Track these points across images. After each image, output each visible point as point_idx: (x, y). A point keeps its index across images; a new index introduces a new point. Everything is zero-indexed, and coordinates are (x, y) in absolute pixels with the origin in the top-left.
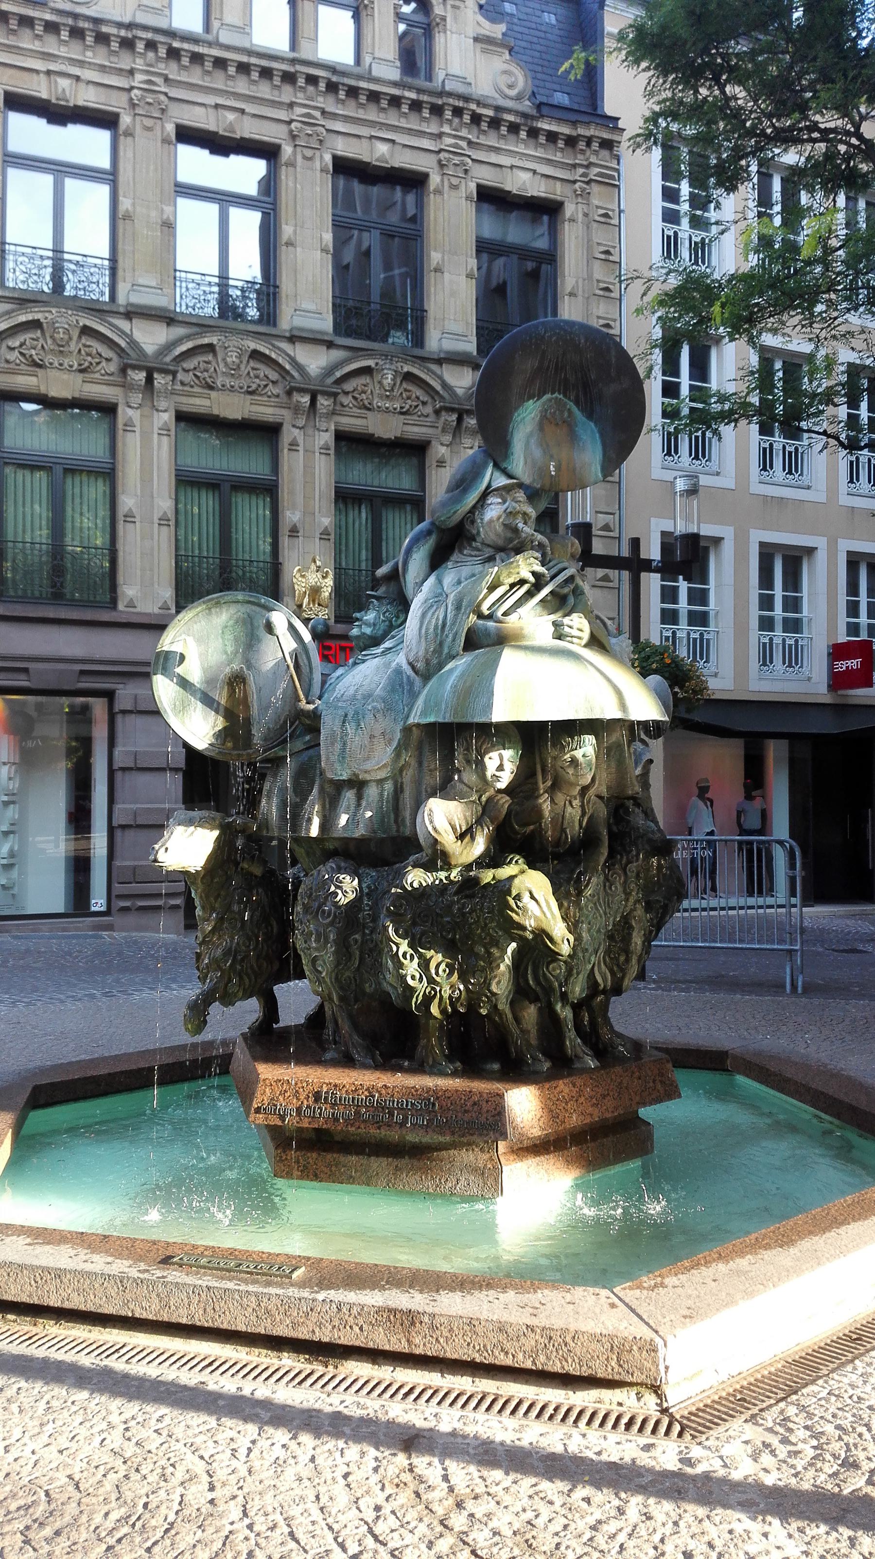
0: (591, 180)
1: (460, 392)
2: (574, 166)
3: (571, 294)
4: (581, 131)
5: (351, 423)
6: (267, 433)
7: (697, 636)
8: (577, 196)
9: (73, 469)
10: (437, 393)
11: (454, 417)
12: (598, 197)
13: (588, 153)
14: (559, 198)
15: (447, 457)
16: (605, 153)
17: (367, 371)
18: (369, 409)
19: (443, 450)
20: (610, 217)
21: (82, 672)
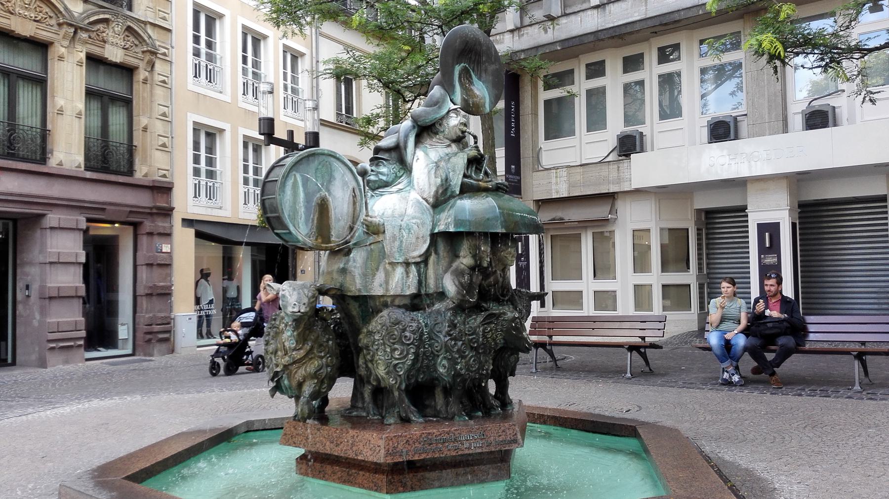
1: (76, 15)
5: (96, 50)
6: (41, 47)
7: (211, 184)
9: (114, 99)
10: (61, 12)
11: (72, 30)
15: (65, 55)
17: (106, 21)
18: (12, 14)
19: (63, 50)
21: (131, 212)
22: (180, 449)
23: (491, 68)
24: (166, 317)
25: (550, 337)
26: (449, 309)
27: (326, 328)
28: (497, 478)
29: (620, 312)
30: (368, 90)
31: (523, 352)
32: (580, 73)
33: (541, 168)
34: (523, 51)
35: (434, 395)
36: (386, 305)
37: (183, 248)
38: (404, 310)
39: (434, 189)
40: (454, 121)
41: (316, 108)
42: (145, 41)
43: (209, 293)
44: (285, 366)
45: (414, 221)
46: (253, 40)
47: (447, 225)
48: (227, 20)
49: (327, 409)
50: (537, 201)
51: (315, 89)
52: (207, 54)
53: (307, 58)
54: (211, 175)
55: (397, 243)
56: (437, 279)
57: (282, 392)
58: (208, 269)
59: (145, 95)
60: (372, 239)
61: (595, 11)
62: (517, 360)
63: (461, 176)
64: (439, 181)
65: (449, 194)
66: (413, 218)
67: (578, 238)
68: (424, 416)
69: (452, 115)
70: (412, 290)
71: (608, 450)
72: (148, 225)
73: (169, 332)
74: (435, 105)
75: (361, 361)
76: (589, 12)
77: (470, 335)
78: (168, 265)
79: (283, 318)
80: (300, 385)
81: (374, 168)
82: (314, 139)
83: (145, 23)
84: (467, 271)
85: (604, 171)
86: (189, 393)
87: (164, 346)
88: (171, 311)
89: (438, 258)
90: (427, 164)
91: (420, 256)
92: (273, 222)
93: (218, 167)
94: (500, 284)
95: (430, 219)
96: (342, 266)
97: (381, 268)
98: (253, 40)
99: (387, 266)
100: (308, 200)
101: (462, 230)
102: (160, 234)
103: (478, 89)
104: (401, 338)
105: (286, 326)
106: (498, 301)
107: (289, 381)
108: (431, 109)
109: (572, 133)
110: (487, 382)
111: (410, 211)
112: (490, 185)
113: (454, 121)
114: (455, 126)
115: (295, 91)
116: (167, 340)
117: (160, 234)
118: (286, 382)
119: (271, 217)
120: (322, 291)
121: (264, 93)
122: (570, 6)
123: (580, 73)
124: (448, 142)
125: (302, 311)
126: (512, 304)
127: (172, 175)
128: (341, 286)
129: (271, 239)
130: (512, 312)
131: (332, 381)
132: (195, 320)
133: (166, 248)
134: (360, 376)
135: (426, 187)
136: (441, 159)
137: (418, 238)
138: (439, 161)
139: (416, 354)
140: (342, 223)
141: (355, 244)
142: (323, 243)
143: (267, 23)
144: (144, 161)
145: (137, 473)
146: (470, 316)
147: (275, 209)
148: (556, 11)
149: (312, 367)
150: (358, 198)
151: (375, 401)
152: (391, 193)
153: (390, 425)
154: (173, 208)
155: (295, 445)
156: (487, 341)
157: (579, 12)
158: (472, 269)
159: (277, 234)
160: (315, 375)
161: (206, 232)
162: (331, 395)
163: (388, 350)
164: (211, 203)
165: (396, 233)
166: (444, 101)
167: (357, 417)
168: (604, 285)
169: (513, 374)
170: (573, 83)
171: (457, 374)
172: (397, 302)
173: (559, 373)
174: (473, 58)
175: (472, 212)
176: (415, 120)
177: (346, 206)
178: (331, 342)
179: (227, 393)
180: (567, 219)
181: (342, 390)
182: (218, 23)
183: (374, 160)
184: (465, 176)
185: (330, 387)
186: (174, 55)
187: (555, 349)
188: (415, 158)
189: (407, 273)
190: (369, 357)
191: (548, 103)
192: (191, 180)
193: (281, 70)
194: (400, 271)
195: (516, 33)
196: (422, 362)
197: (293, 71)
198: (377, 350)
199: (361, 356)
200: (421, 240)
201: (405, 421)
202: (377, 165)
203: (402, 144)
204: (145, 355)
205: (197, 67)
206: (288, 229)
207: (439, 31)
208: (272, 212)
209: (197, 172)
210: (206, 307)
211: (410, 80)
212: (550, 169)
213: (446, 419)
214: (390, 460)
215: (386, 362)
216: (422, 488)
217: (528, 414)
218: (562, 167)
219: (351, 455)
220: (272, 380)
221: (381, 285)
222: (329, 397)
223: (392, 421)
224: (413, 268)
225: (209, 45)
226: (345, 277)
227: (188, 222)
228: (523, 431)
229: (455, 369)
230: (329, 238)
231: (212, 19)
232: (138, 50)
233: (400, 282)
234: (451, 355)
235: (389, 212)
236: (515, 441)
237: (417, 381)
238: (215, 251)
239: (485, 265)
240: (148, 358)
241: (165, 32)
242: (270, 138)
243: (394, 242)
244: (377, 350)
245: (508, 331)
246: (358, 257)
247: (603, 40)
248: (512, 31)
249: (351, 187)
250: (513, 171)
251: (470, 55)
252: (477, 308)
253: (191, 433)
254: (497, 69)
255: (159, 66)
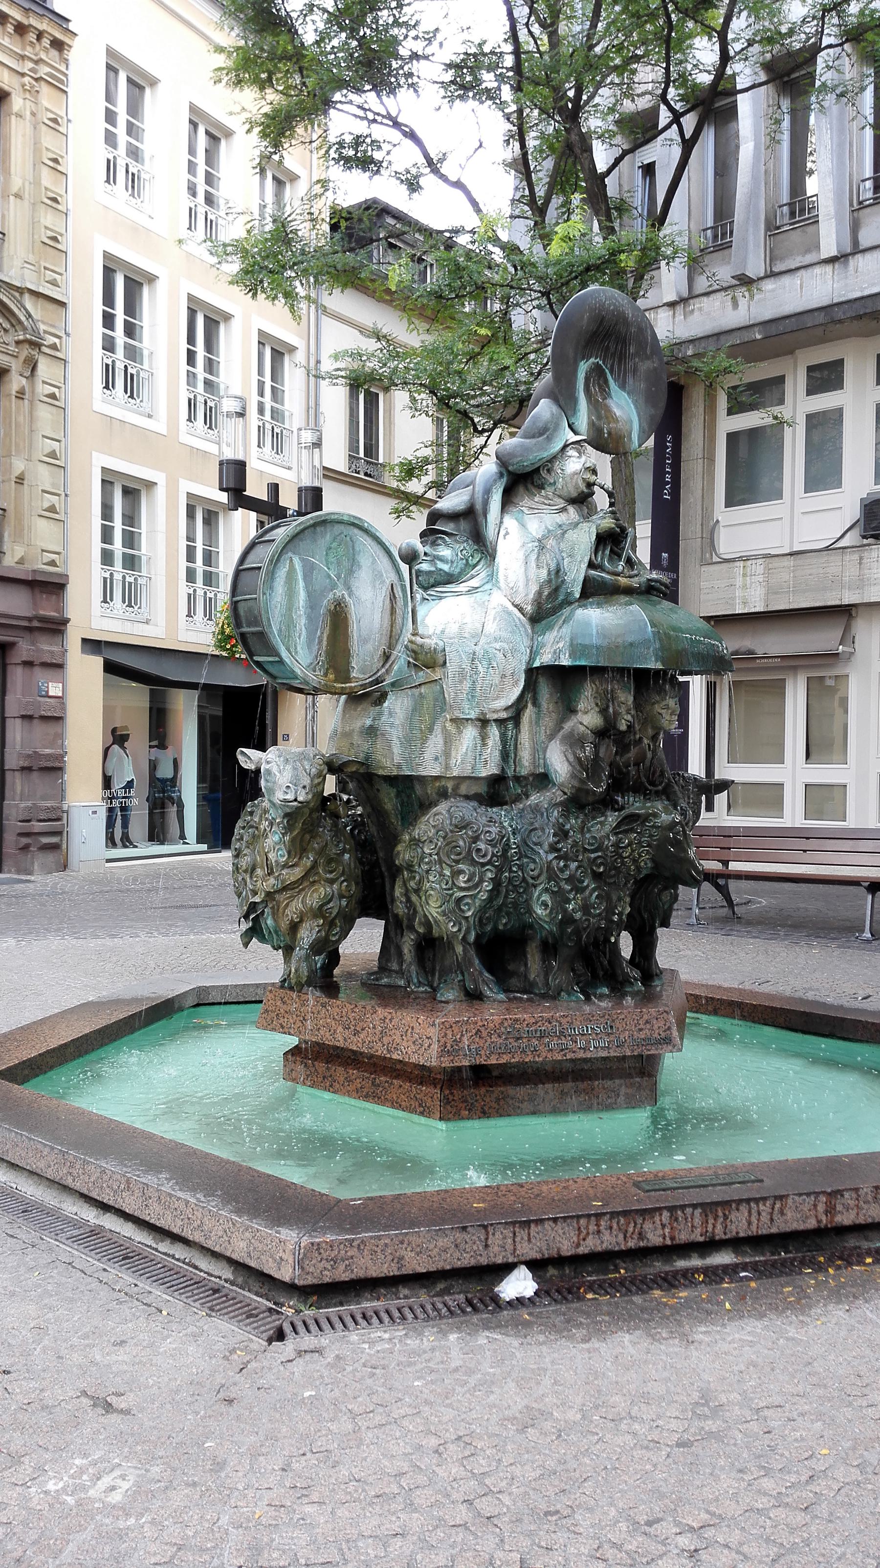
0: (41, 78)
2: (23, 57)
3: (17, 196)
4: (33, 21)
7: (132, 580)
8: (25, 90)
12: (47, 97)
13: (38, 47)
14: (6, 88)
16: (54, 53)
20: (58, 124)
22: (87, 1031)
23: (645, 366)
24: (54, 809)
25: (726, 863)
26: (556, 805)
27: (337, 831)
28: (632, 1104)
29: (852, 822)
30: (408, 413)
31: (685, 884)
32: (796, 383)
33: (715, 559)
34: (692, 341)
35: (524, 954)
36: (443, 794)
37: (83, 693)
38: (476, 804)
39: (534, 588)
40: (573, 464)
41: (318, 444)
42: (20, 322)
43: (128, 768)
44: (269, 894)
45: (498, 645)
46: (206, 324)
47: (557, 654)
48: (161, 286)
49: (336, 971)
50: (708, 619)
51: (312, 412)
52: (127, 347)
53: (300, 356)
54: (131, 562)
55: (467, 685)
56: (534, 751)
57: (262, 939)
58: (126, 728)
59: (21, 419)
60: (421, 676)
61: (829, 268)
62: (675, 898)
63: (584, 566)
64: (544, 574)
65: (561, 598)
66: (496, 640)
67: (778, 689)
68: (506, 991)
69: (571, 452)
70: (491, 769)
71: (830, 1063)
72: (24, 648)
73: (59, 833)
74: (541, 435)
75: (398, 892)
76: (818, 270)
77: (593, 851)
78: (59, 719)
79: (266, 811)
80: (294, 927)
81: (427, 549)
82: (313, 498)
83: (21, 290)
84: (591, 737)
85: (834, 565)
86: (97, 937)
87: (50, 858)
88: (63, 798)
89: (538, 714)
90: (525, 543)
91: (507, 709)
92: (251, 641)
93: (144, 549)
94: (647, 762)
95: (527, 642)
96: (368, 722)
97: (438, 729)
98: (206, 324)
99: (448, 724)
100: (312, 605)
101: (583, 663)
102: (45, 665)
103: (618, 406)
104: (469, 852)
105: (271, 824)
106: (638, 789)
107: (275, 920)
108: (534, 441)
109: (778, 494)
110: (619, 935)
111: (491, 628)
112: (635, 582)
113: (573, 464)
114: (575, 473)
115: (277, 415)
116: (56, 847)
117: (45, 665)
118: (270, 922)
119: (246, 632)
120: (332, 767)
121: (229, 415)
122: (782, 259)
123: (796, 383)
124: (562, 504)
125: (300, 799)
126: (668, 799)
127: (65, 562)
128: (367, 758)
129: (237, 678)
130: (668, 812)
131: (346, 922)
132: (103, 814)
133: (55, 689)
134: (396, 916)
135: (521, 584)
136: (549, 533)
137: (503, 676)
138: (545, 537)
139: (497, 882)
140: (369, 647)
141: (393, 684)
142: (336, 680)
143: (235, 288)
144: (19, 535)
145: (16, 1066)
146: (594, 818)
147: (256, 620)
148: (755, 267)
149: (314, 897)
150: (400, 602)
151: (420, 962)
152: (459, 594)
153: (447, 1002)
154: (67, 621)
155: (284, 1030)
156: (623, 863)
157: (798, 269)
158: (601, 734)
159: (258, 664)
160: (319, 912)
161: (122, 664)
162: (345, 948)
163: (447, 873)
164: (130, 613)
165: (466, 666)
166: (557, 427)
167: (389, 986)
168: (823, 774)
169: (665, 924)
170: (781, 402)
171: (568, 920)
172: (464, 789)
173: (738, 927)
174: (612, 350)
175: (603, 633)
176: (502, 460)
177: (377, 617)
178: (347, 856)
179: (160, 940)
180: (760, 652)
181: (364, 941)
182: (146, 290)
183: (429, 535)
184: (591, 565)
185: (344, 934)
186: (71, 349)
187: (733, 885)
188: (502, 532)
189: (484, 737)
190: (412, 884)
191: (733, 438)
192: (98, 572)
193: (255, 377)
194: (470, 733)
195: (679, 309)
196: (506, 897)
197: (274, 378)
198: (427, 872)
199: (399, 883)
200: (508, 681)
201: (474, 996)
202: (434, 544)
203: (479, 507)
204: (18, 872)
205: (109, 371)
206: (278, 655)
207: (544, 301)
208: (248, 626)
209: (107, 558)
210: (121, 793)
211: (484, 393)
212: (733, 560)
213: (544, 997)
214: (446, 1063)
215: (443, 893)
216: (501, 1113)
217: (689, 996)
218: (756, 557)
219: (380, 1050)
220: (246, 917)
221: (436, 759)
222: (341, 951)
223: (450, 995)
224: (494, 732)
225: (130, 330)
226: (374, 743)
227: (92, 645)
228: (681, 1024)
229: (565, 911)
230: (348, 672)
231: (136, 283)
232: (10, 338)
233: (470, 755)
234: (557, 885)
235: (453, 629)
236: (667, 1041)
237: (495, 928)
238: (136, 697)
239: (623, 727)
240: (23, 877)
241: (55, 306)
242: (239, 497)
243: (461, 682)
244: (427, 872)
245: (660, 847)
246: (397, 707)
247: (840, 321)
248: (672, 305)
249: (388, 582)
250: (665, 563)
251: (608, 342)
252: (606, 803)
253: (103, 1003)
254: (655, 369)
255: (44, 368)
